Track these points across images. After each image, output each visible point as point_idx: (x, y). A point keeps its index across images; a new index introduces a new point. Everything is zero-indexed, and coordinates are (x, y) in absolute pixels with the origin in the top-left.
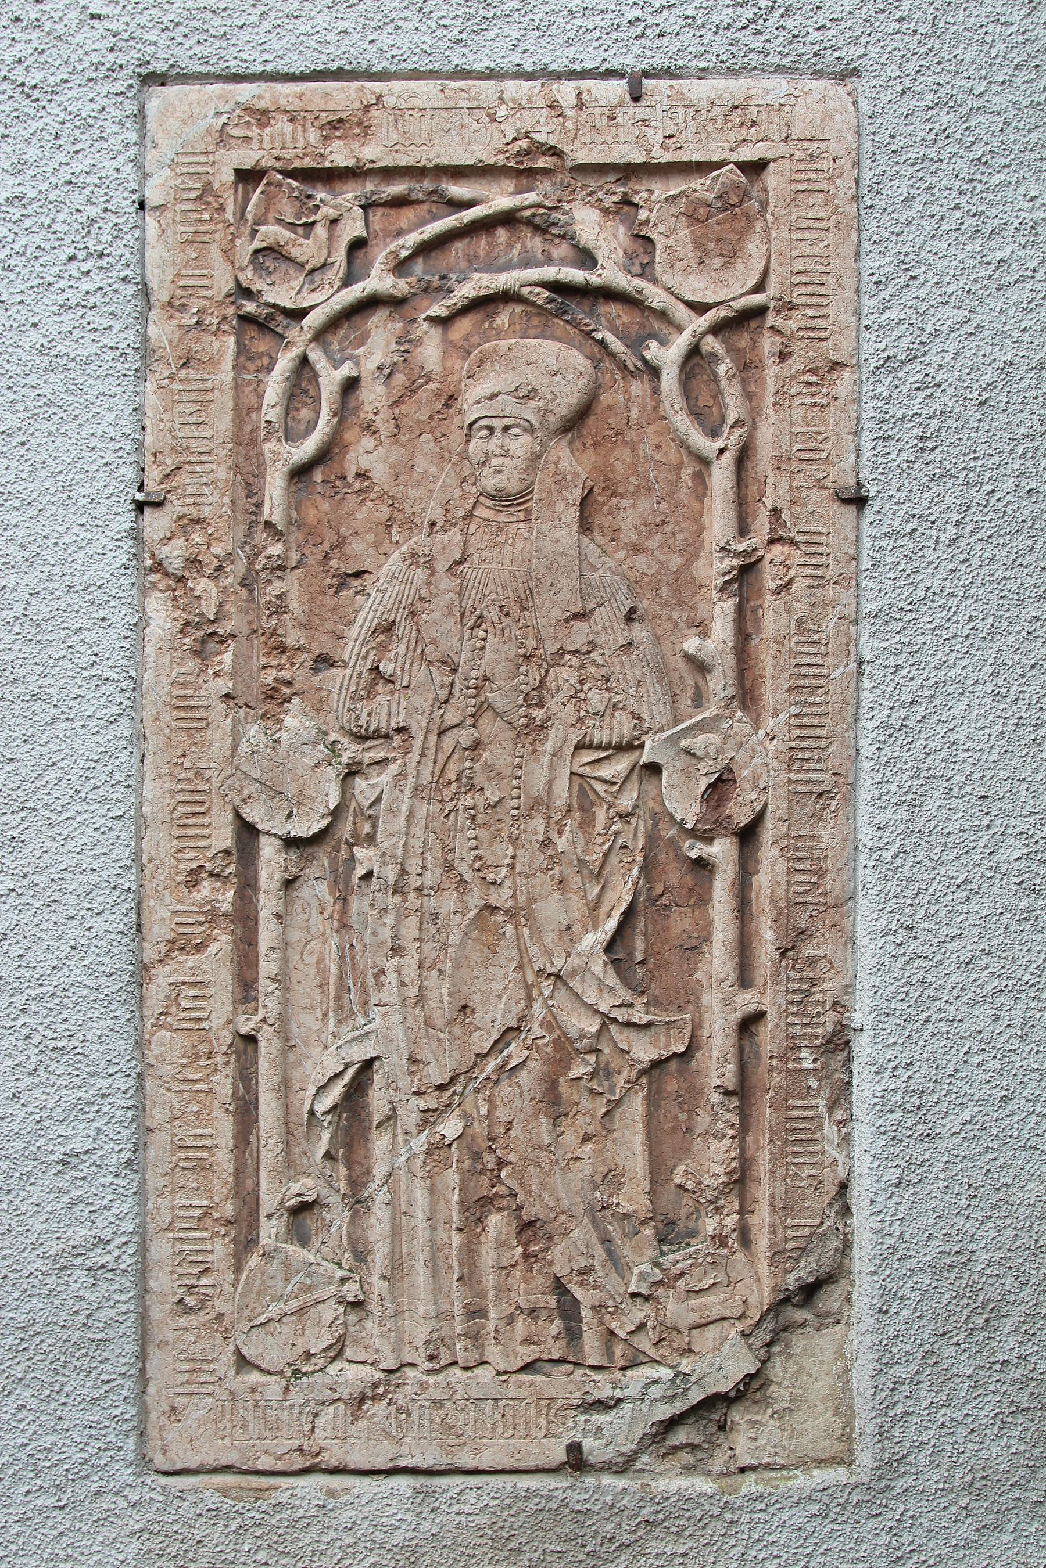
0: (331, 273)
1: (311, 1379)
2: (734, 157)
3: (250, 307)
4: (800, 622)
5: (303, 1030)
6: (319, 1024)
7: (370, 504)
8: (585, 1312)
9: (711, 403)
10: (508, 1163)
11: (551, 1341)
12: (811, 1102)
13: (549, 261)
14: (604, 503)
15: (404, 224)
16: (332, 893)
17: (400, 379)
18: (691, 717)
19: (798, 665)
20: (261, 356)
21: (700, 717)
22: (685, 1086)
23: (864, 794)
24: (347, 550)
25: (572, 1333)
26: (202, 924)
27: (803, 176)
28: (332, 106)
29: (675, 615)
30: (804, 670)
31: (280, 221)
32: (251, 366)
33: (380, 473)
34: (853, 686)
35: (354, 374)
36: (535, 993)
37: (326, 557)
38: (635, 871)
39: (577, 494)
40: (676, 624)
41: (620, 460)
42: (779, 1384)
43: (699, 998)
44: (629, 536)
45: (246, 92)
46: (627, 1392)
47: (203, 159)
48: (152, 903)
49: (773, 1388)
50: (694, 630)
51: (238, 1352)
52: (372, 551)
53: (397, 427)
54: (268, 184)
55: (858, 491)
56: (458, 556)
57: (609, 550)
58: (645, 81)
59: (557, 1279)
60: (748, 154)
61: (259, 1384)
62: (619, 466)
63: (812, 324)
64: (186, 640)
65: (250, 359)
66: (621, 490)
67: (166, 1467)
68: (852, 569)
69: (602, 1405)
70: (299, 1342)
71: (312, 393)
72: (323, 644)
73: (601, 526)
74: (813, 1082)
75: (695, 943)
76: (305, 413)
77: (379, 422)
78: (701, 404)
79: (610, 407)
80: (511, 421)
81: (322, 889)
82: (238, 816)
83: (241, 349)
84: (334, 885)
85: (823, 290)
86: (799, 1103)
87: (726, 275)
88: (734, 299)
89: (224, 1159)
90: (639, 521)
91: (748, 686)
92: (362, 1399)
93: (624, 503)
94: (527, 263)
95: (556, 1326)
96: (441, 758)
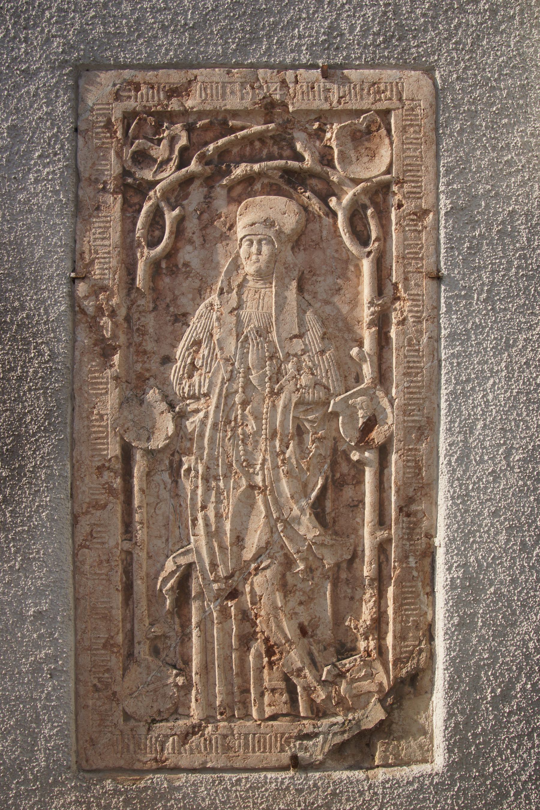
0: (172, 163)
1: (161, 724)
2: (374, 107)
3: (130, 180)
4: (410, 340)
5: (156, 548)
6: (164, 545)
7: (190, 279)
8: (299, 689)
9: (363, 229)
10: (260, 616)
11: (282, 704)
12: (414, 584)
13: (281, 157)
14: (309, 279)
15: (208, 139)
16: (170, 478)
17: (206, 216)
18: (354, 388)
19: (408, 362)
20: (135, 204)
21: (359, 388)
22: (350, 575)
23: (443, 427)
24: (179, 302)
25: (293, 700)
26: (102, 494)
27: (409, 118)
28: (172, 81)
29: (346, 336)
30: (411, 365)
31: (145, 138)
32: (131, 210)
33: (195, 264)
34: (436, 373)
35: (183, 213)
36: (274, 529)
37: (168, 306)
38: (326, 467)
39: (296, 274)
40: (346, 340)
41: (317, 257)
42: (397, 724)
43: (357, 531)
44: (322, 295)
45: (127, 74)
46: (320, 729)
47: (107, 107)
48: (78, 483)
49: (394, 725)
50: (356, 344)
51: (124, 710)
52: (191, 303)
53: (204, 240)
54: (140, 119)
55: (438, 274)
56: (235, 305)
57: (312, 303)
58: (329, 71)
59: (285, 674)
60: (380, 106)
61: (135, 727)
62: (317, 260)
63: (415, 190)
64: (96, 348)
65: (131, 206)
66: (318, 272)
67: (88, 768)
68: (435, 313)
69: (308, 736)
70: (155, 705)
71: (161, 223)
72: (165, 351)
73: (308, 291)
74: (415, 574)
75: (356, 503)
76: (157, 233)
77: (195, 238)
78: (358, 229)
79: (312, 230)
80: (262, 237)
81: (166, 476)
82: (122, 438)
83: (125, 201)
84: (171, 475)
85: (419, 174)
86: (408, 584)
87: (370, 165)
88: (375, 177)
89: (118, 613)
90: (327, 288)
91: (383, 372)
92: (187, 734)
93: (319, 279)
94: (271, 157)
95: (285, 697)
96: (227, 409)
